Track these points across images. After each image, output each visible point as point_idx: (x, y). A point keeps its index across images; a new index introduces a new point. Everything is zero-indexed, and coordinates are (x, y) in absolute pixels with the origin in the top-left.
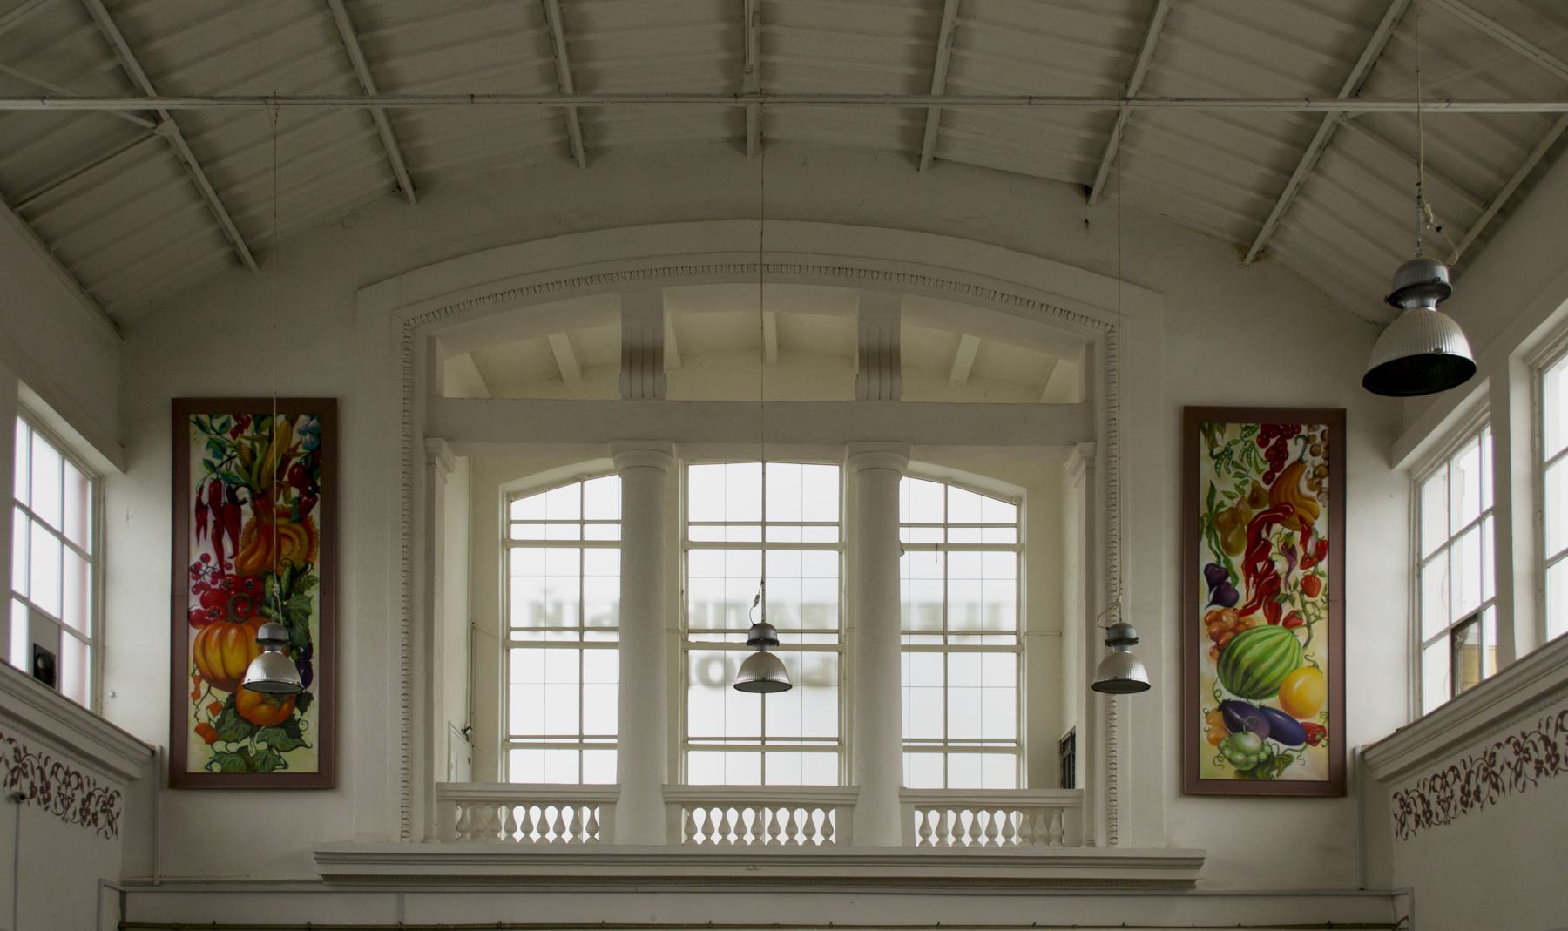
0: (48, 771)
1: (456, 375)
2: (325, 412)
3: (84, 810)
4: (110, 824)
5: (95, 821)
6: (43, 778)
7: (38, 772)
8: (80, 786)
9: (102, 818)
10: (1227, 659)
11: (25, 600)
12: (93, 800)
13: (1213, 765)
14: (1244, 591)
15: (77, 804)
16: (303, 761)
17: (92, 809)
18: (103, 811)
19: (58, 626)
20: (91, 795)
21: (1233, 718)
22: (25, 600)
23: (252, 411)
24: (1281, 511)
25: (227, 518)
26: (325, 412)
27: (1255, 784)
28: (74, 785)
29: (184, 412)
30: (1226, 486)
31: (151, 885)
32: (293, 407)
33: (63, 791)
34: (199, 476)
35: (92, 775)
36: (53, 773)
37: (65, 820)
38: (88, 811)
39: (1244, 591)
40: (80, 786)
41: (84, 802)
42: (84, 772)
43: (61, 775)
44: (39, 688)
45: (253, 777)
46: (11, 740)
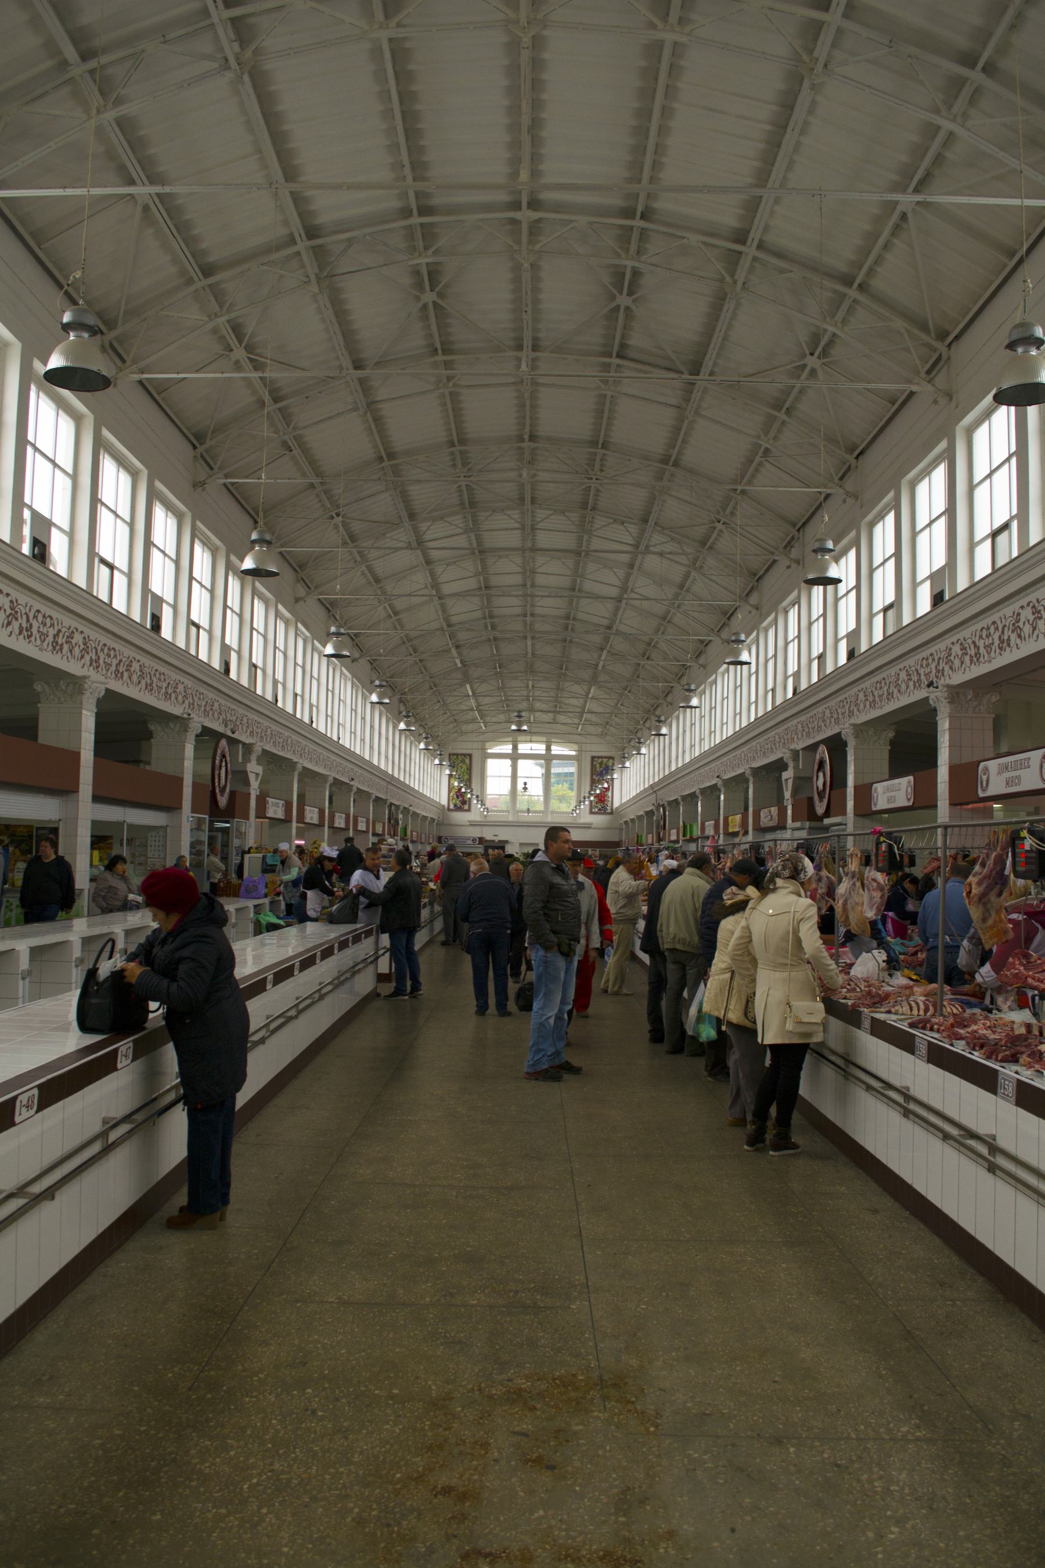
3: (55, 643)
4: (71, 651)
5: (61, 650)
6: (28, 620)
7: (24, 617)
12: (61, 635)
28: (48, 624)
38: (57, 643)
40: (52, 625)
43: (40, 618)
44: (152, 634)
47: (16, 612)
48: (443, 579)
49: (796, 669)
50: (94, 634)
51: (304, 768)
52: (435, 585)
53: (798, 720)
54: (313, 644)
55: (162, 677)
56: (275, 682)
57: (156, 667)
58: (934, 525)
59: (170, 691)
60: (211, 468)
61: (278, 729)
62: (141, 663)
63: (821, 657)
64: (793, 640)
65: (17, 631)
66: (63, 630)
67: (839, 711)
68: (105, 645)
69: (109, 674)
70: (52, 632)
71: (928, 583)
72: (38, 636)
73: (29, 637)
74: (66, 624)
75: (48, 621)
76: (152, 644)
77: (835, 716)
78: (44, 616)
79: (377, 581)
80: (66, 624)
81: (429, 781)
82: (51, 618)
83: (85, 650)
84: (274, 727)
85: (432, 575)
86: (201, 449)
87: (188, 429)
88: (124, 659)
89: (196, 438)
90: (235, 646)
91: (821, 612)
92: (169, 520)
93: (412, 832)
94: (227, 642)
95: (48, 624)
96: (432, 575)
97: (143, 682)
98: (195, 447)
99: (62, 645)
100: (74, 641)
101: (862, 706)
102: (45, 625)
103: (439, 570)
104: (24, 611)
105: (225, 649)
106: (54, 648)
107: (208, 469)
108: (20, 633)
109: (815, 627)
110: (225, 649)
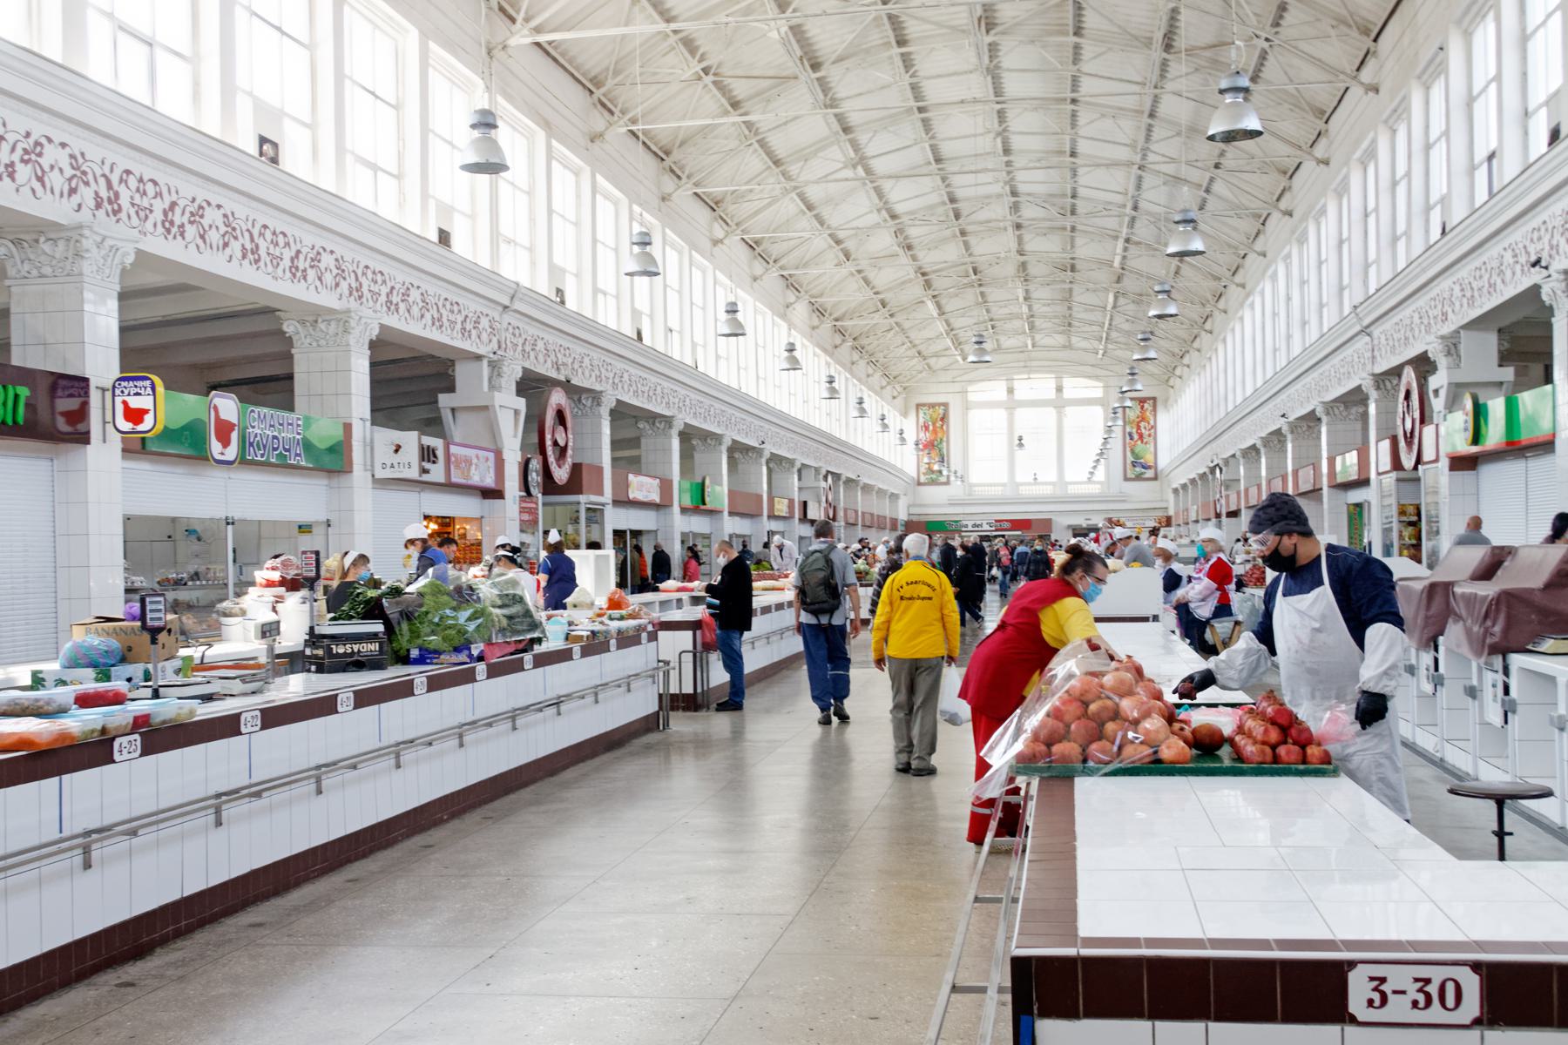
0: (256, 232)
1: (972, 397)
2: (946, 405)
3: (294, 268)
4: (320, 279)
5: (182, 234)
6: (252, 240)
7: (247, 235)
8: (159, 195)
9: (311, 274)
10: (1132, 451)
11: (250, 94)
12: (302, 257)
13: (1130, 475)
14: (1136, 437)
15: (286, 263)
16: (943, 479)
17: (178, 220)
18: (191, 223)
19: (278, 115)
20: (173, 205)
21: (1134, 464)
22: (250, 94)
23: (932, 406)
24: (1143, 419)
25: (927, 428)
26: (946, 405)
27: (1139, 478)
28: (281, 243)
29: (918, 406)
30: (1132, 415)
31: (914, 505)
32: (940, 405)
33: (137, 200)
34: (921, 421)
35: (173, 182)
36: (121, 180)
37: (276, 278)
38: (172, 223)
39: (1136, 437)
40: (287, 244)
41: (292, 260)
42: (546, 337)
43: (268, 235)
44: (441, 250)
45: (933, 482)
46: (63, 145)
47: (84, 173)
48: (870, 150)
49: (1445, 191)
50: (431, 287)
51: (734, 441)
52: (862, 161)
53: (1413, 307)
54: (664, 234)
55: (456, 308)
56: (694, 345)
57: (560, 342)
58: (1550, 23)
59: (528, 348)
60: (612, 113)
61: (640, 373)
62: (422, 290)
63: (1444, 201)
64: (1439, 139)
65: (239, 254)
66: (304, 250)
67: (1475, 285)
68: (265, 227)
69: (149, 225)
70: (384, 290)
71: (1544, 111)
72: (132, 211)
73: (257, 261)
74: (400, 278)
75: (281, 239)
76: (557, 317)
77: (1469, 294)
78: (274, 233)
79: (777, 163)
80: (400, 278)
81: (884, 441)
82: (285, 235)
83: (231, 231)
84: (665, 384)
85: (855, 146)
86: (598, 93)
87: (583, 75)
88: (397, 286)
89: (590, 84)
90: (646, 310)
91: (1492, 72)
92: (605, 209)
93: (846, 510)
94: (637, 306)
95: (281, 243)
96: (855, 146)
97: (428, 316)
98: (591, 92)
99: (304, 271)
100: (322, 266)
101: (1508, 273)
102: (277, 244)
103: (863, 138)
104: (98, 172)
105: (636, 314)
106: (168, 231)
107: (606, 113)
108: (244, 257)
109: (1434, 153)
110: (636, 314)
